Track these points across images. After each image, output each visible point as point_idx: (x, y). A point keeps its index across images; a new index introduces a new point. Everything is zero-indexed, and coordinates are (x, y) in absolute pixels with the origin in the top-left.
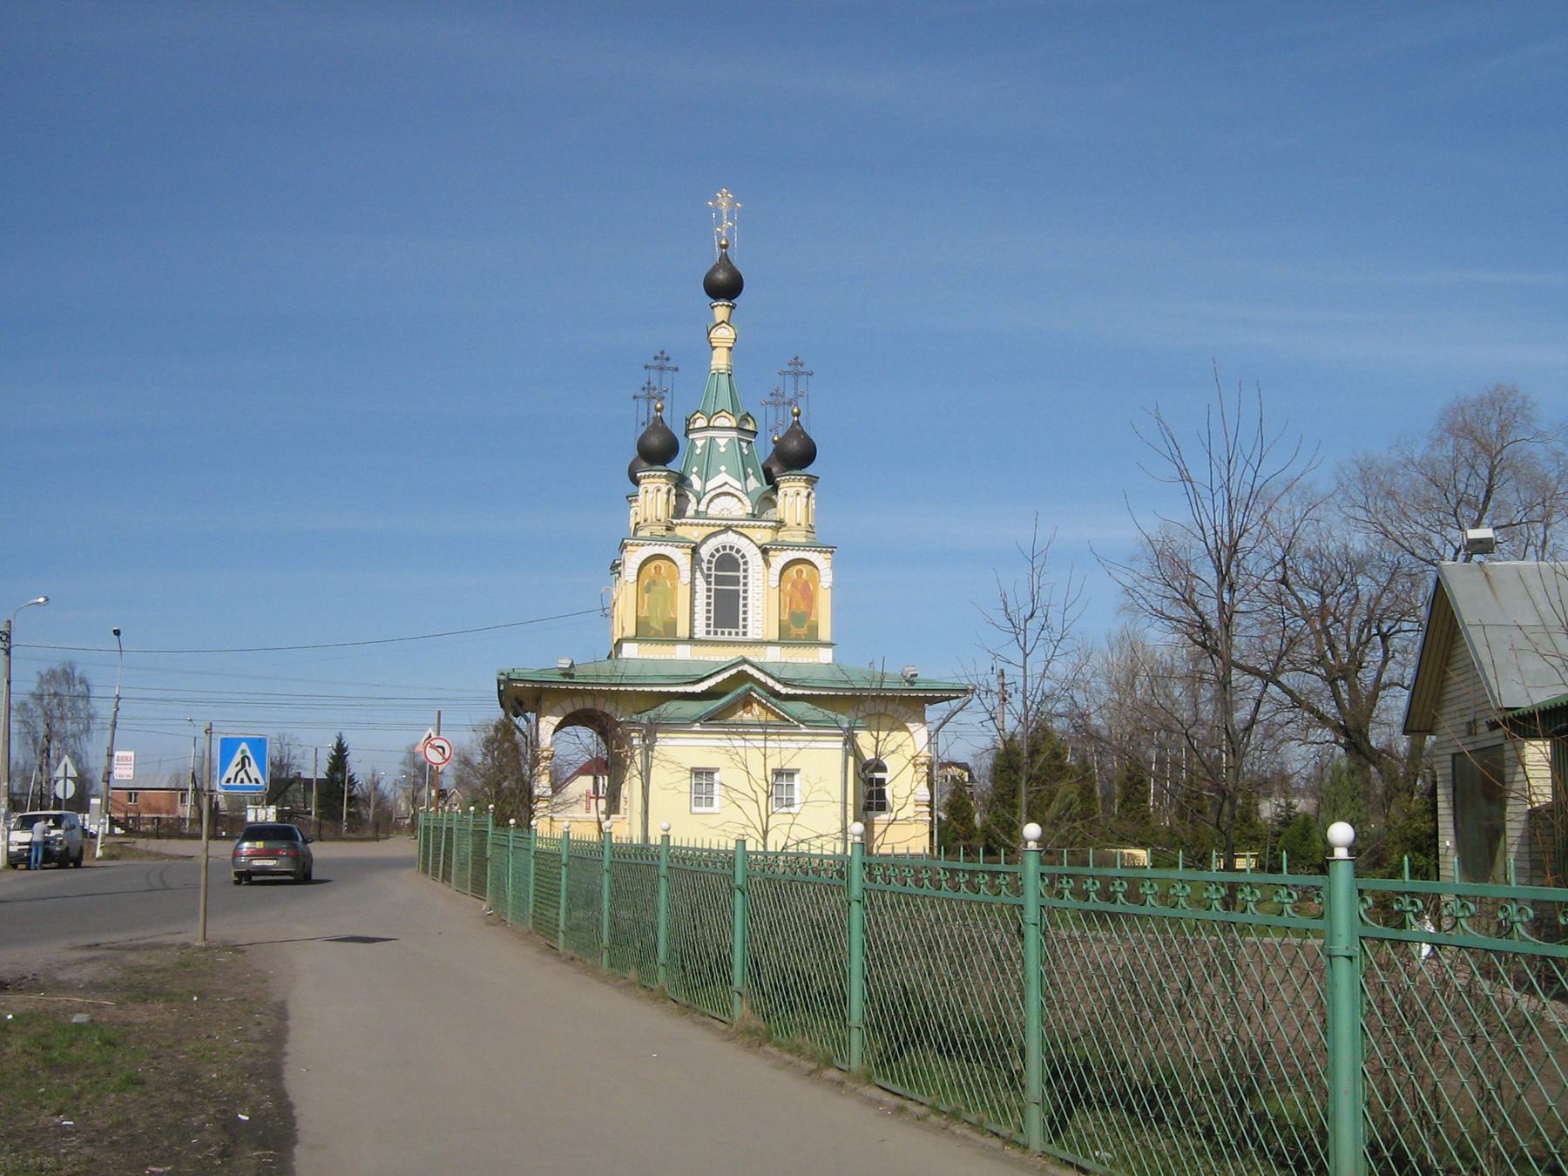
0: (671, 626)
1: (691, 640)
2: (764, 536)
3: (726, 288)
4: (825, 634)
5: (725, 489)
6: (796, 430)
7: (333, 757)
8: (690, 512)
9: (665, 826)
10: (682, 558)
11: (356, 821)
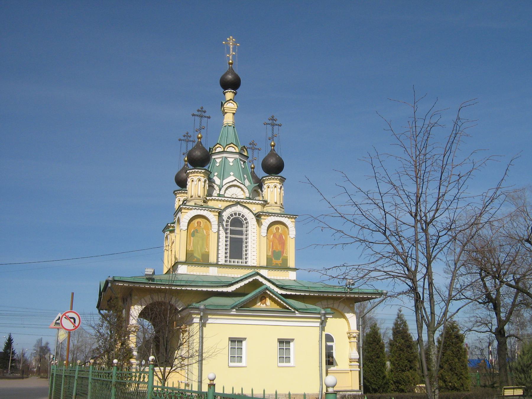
0: (206, 256)
1: (217, 265)
2: (257, 209)
3: (232, 84)
4: (292, 263)
5: (235, 183)
6: (273, 153)
7: (7, 343)
8: (215, 193)
9: (211, 376)
10: (213, 217)
11: (14, 369)
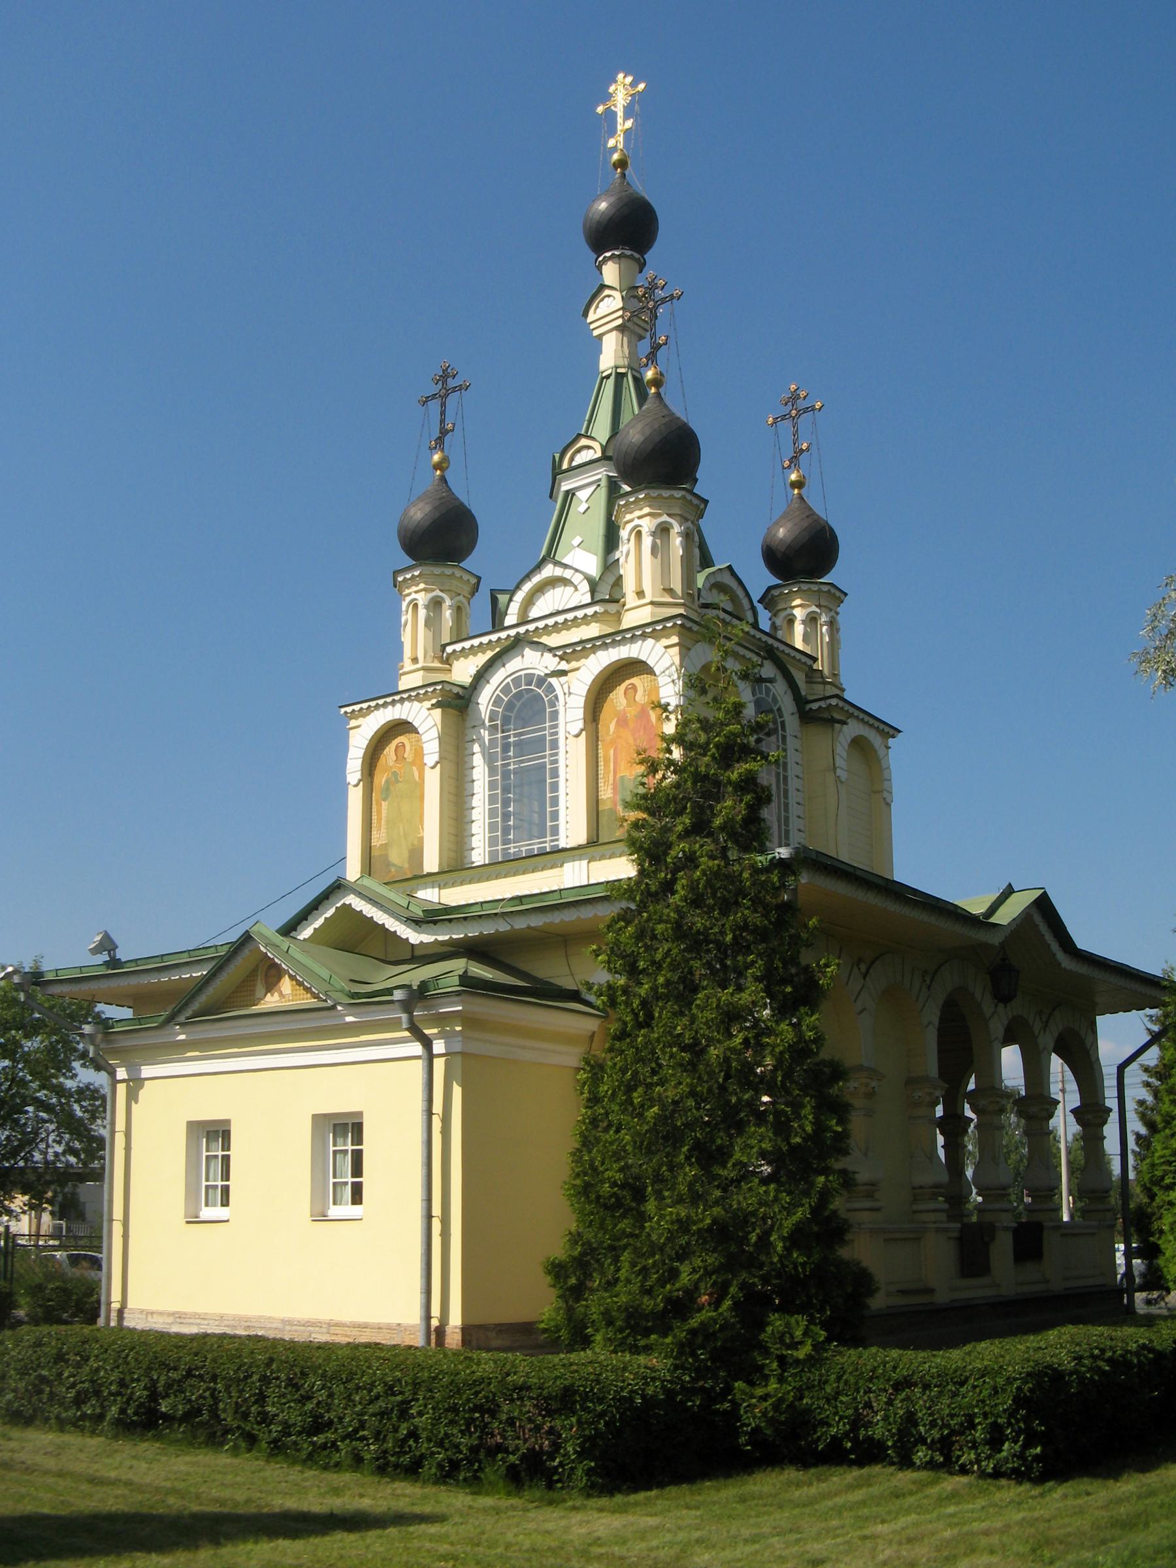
3: (629, 229)
